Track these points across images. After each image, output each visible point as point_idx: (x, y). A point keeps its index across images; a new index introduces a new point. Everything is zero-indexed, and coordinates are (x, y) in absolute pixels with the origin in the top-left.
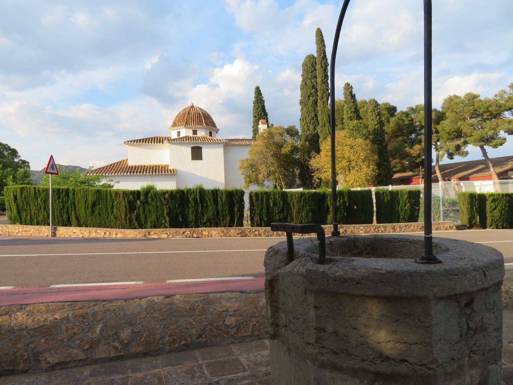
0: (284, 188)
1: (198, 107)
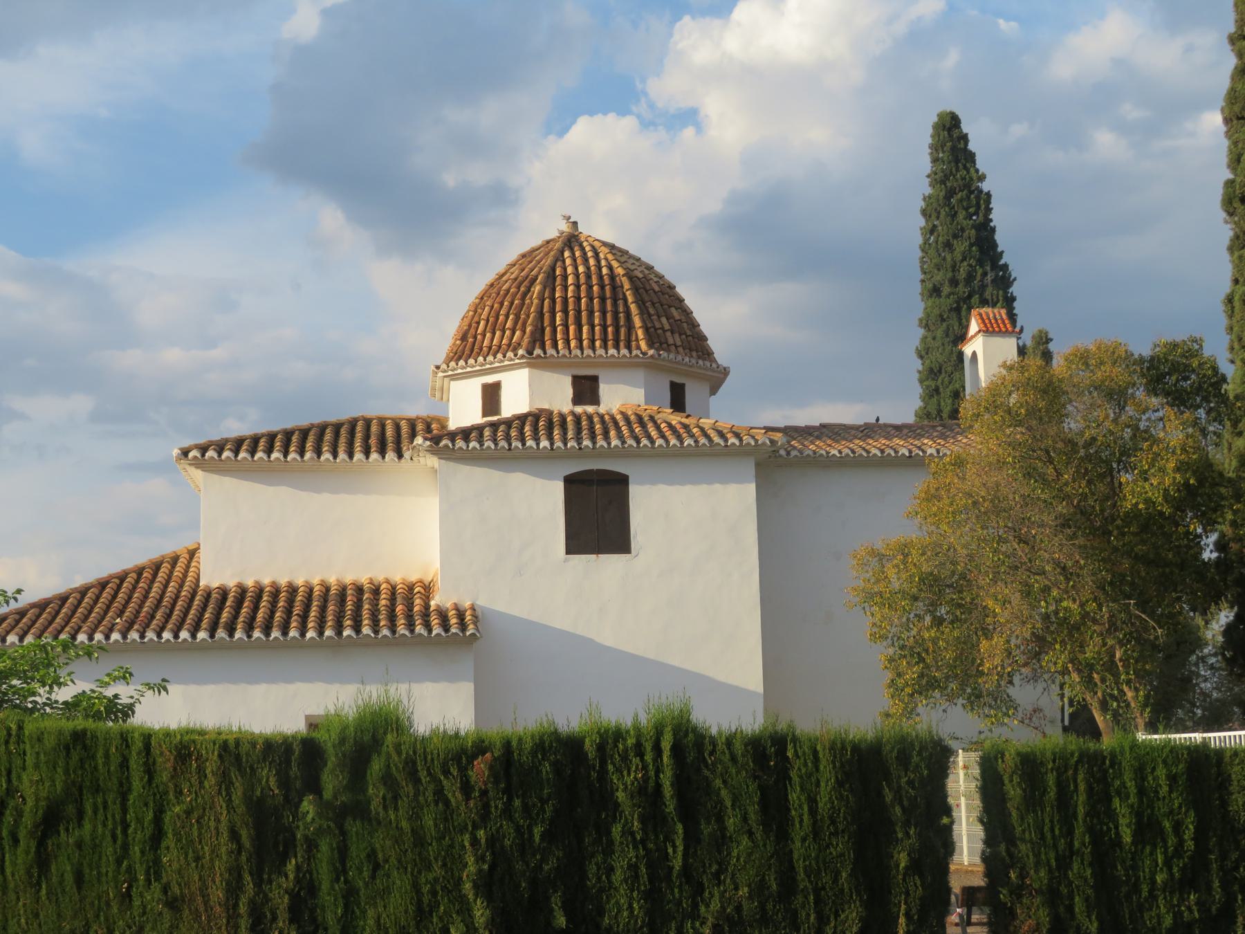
1: (605, 244)
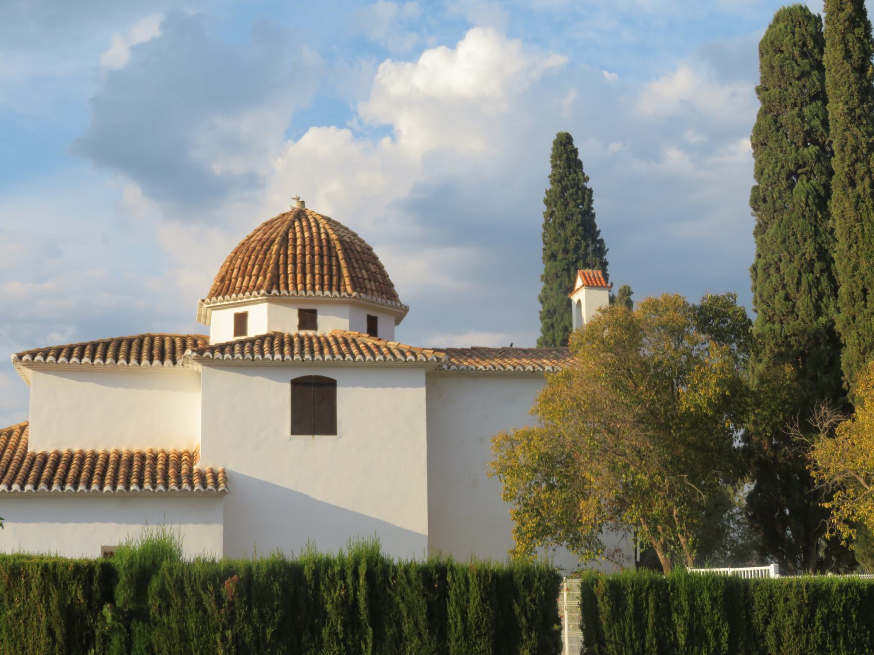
0: (689, 559)
1: (324, 217)
